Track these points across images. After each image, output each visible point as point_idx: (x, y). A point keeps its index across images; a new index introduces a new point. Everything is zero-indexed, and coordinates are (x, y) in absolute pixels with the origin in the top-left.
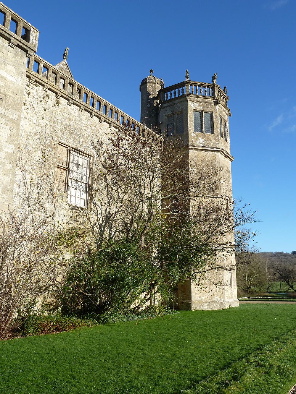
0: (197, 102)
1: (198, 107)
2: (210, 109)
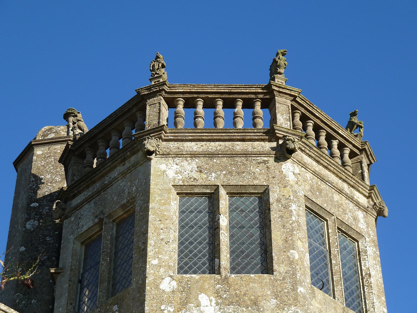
0: (194, 155)
1: (195, 175)
2: (255, 178)
